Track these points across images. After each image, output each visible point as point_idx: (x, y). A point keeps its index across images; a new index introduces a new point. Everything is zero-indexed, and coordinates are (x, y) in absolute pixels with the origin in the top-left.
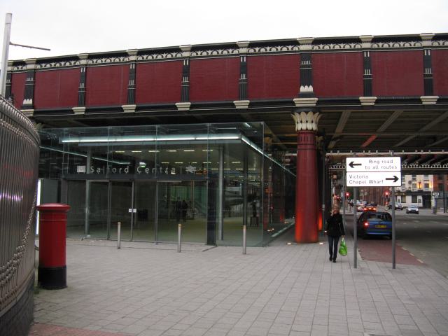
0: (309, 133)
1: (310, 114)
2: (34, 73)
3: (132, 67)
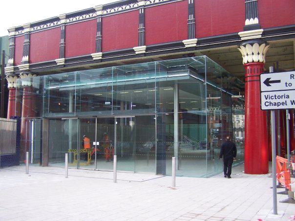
0: (256, 65)
1: (256, 45)
2: (29, 35)
3: (141, 11)
